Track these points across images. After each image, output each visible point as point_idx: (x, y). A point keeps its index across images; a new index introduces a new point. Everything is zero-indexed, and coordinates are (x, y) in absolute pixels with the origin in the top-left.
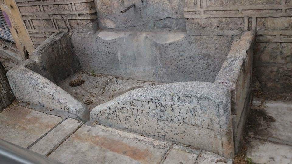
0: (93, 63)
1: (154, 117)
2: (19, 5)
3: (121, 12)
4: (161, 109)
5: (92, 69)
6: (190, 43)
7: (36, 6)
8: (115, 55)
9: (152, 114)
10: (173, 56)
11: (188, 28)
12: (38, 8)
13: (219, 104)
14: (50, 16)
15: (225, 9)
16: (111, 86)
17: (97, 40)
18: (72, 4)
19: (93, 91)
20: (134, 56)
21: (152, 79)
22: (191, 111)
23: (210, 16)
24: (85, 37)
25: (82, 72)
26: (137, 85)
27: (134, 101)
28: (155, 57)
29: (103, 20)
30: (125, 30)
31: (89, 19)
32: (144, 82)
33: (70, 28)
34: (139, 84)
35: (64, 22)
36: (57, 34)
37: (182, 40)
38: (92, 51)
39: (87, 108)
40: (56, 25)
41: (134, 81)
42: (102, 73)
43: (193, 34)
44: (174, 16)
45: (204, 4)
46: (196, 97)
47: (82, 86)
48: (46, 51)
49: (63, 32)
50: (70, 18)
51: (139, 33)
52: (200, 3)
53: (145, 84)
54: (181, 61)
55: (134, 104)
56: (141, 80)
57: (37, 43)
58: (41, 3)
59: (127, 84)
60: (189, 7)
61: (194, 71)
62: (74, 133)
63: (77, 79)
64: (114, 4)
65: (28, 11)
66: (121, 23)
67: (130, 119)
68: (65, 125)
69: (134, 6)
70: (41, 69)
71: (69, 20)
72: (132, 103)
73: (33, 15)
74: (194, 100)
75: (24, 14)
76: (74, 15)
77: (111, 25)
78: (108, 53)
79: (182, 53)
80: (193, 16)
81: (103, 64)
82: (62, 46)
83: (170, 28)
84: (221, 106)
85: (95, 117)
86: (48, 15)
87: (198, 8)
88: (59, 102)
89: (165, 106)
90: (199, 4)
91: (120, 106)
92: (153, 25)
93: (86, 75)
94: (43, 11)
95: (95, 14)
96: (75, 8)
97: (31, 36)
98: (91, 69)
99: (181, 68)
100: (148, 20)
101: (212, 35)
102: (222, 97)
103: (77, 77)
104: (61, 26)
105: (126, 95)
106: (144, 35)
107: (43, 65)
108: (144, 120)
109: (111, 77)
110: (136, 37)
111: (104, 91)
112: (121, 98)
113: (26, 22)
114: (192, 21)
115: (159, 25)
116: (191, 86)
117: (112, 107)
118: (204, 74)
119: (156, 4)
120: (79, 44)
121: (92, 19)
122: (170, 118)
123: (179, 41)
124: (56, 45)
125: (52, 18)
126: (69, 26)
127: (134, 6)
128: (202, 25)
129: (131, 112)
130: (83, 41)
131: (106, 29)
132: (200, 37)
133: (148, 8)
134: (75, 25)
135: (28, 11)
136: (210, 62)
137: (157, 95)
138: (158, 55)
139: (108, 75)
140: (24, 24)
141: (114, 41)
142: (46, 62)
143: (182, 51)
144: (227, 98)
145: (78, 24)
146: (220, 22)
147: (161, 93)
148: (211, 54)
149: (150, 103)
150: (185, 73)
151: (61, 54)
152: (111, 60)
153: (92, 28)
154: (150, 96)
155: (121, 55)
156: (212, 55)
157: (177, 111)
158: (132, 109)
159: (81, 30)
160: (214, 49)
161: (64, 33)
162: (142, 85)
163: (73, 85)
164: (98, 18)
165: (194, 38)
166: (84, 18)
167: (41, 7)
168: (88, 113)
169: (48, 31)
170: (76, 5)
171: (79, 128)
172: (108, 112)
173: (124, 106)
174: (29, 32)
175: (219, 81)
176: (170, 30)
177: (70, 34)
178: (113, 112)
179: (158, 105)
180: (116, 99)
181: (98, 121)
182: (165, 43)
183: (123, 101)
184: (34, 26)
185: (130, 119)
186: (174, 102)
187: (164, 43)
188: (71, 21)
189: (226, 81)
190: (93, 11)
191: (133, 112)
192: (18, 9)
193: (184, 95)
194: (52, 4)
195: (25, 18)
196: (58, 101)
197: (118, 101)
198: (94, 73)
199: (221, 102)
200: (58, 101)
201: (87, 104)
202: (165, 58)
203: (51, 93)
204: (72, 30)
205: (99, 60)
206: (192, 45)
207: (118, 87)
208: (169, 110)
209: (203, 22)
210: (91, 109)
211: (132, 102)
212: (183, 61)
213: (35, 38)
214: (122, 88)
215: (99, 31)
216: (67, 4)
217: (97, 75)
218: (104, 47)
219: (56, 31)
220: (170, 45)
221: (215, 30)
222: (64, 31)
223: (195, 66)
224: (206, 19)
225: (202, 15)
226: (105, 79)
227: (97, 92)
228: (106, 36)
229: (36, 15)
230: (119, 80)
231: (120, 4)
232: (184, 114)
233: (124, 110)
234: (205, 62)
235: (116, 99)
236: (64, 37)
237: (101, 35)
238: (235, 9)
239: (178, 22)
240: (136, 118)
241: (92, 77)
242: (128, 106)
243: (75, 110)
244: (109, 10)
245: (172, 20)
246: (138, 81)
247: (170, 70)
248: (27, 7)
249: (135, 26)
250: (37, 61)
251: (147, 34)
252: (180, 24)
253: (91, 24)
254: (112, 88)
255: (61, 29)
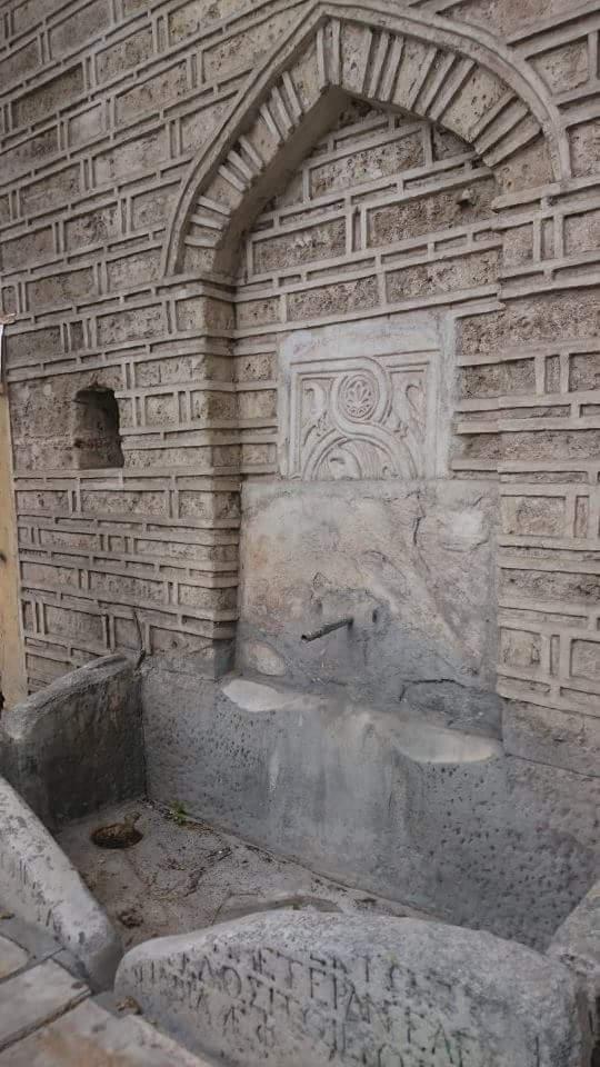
0: (188, 775)
1: (322, 1033)
2: (25, 557)
3: (304, 637)
4: (348, 1010)
5: (180, 796)
6: (512, 782)
7: (70, 569)
8: (262, 764)
9: (315, 1019)
10: (449, 814)
11: (505, 728)
12: (75, 577)
13: (540, 1039)
14: (103, 605)
16: (222, 874)
17: (216, 704)
18: (171, 584)
19: (159, 878)
20: (321, 781)
21: (368, 881)
22: (448, 1045)
24: (185, 687)
25: (146, 800)
26: (314, 891)
27: (265, 954)
28: (391, 801)
29: (251, 645)
30: (309, 687)
31: (211, 636)
32: (339, 886)
33: (148, 651)
34: (320, 888)
35: (135, 631)
36: (105, 664)
37: (487, 766)
39: (117, 938)
41: (305, 874)
42: (205, 817)
43: (521, 752)
44: (468, 680)
46: (468, 991)
47: (130, 853)
48: (56, 711)
49: (125, 659)
51: (349, 709)
53: (341, 892)
54: (475, 839)
55: (264, 966)
56: (331, 874)
57: (38, 677)
59: (278, 877)
60: (517, 666)
61: (518, 888)
62: (47, 1022)
63: (123, 822)
64: (291, 605)
65: (44, 579)
67: (242, 1019)
68: (28, 986)
70: (20, 768)
71: (152, 627)
72: (257, 958)
73: (55, 593)
74: (462, 1003)
75: (28, 584)
79: (480, 810)
80: (526, 697)
81: (216, 787)
82: (110, 702)
83: (451, 713)
84: (545, 1050)
85: (131, 978)
86: (95, 601)
87: (542, 676)
88: (39, 894)
89: (362, 1001)
90: (545, 664)
91: (218, 961)
92: (398, 693)
93: (156, 814)
95: (233, 624)
97: (29, 651)
98: (175, 796)
99: (476, 863)
102: (552, 1015)
103: (123, 814)
105: (246, 924)
106: (365, 718)
107: (30, 753)
108: (290, 1039)
109: (232, 840)
110: (340, 718)
111: (194, 886)
112: (227, 932)
113: (28, 606)
114: (522, 712)
116: (461, 946)
117: (191, 958)
118: (554, 906)
119: (413, 632)
121: (216, 637)
122: (375, 1054)
123: (473, 765)
124: (91, 697)
126: (146, 646)
127: (350, 623)
128: (554, 732)
129: (250, 995)
131: (255, 674)
132: (545, 768)
134: (166, 645)
135: (44, 579)
136: (577, 869)
137: (343, 952)
138: (401, 797)
139: (225, 831)
140: (21, 612)
141: (268, 717)
142: (43, 749)
143: (483, 803)
144: (571, 1021)
145: (175, 644)
147: (359, 945)
148: (578, 837)
149: (318, 977)
150: (485, 885)
151: (96, 729)
152: (247, 777)
153: (212, 665)
154: (321, 948)
155: (281, 769)
156: (583, 842)
157: (400, 1029)
158: (255, 984)
159: (177, 665)
161: (125, 663)
162: (332, 897)
163: (105, 841)
165: (525, 769)
167: (85, 575)
168: (114, 956)
169: (81, 646)
170: (183, 588)
171: (69, 1007)
172: (177, 974)
173: (232, 963)
174: (26, 638)
175: (561, 951)
176: (451, 722)
177: (144, 669)
178: (193, 976)
179: (341, 991)
180: (211, 932)
181: (138, 999)
182: (427, 760)
183: (231, 944)
184: (48, 623)
185: (242, 1019)
186: (396, 994)
187: (424, 759)
189: (583, 957)
190: (228, 616)
191: (254, 995)
192: (18, 567)
193: (431, 974)
195: (28, 597)
196: (37, 890)
197: (216, 941)
198: (182, 812)
199: (549, 1033)
200: (37, 890)
201: (124, 923)
203: (24, 858)
206: (516, 790)
207: (247, 885)
208: (376, 1018)
209: (558, 722)
210: (130, 943)
211: (260, 956)
212: (484, 838)
213: (40, 661)
215: (229, 676)
216: (159, 583)
217: (191, 823)
218: (232, 728)
219: (106, 651)
220: (443, 770)
222: (129, 656)
223: (522, 868)
224: (566, 716)
225: (554, 699)
226: (211, 843)
227: (172, 884)
228: (248, 697)
230: (254, 858)
231: (308, 611)
232: (424, 1049)
233: (227, 978)
234: (560, 860)
235: (212, 931)
236: (123, 676)
237: (234, 690)
239: (481, 703)
240: (261, 1022)
241: (172, 826)
242: (243, 967)
243: (78, 938)
244: (274, 622)
246: (318, 878)
247: (435, 861)
248: (43, 567)
249: (344, 684)
250: (17, 736)
252: (486, 710)
253: (211, 653)
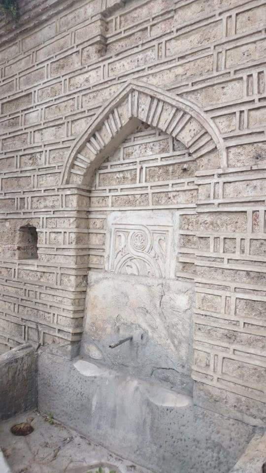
3: (110, 346)
5: (51, 410)
6: (196, 417)
7: (10, 303)
8: (89, 400)
11: (195, 393)
12: (12, 307)
15: (246, 384)
17: (70, 371)
18: (54, 314)
21: (133, 457)
23: (226, 387)
24: (57, 361)
28: (145, 422)
30: (111, 367)
31: (70, 340)
33: (42, 344)
35: (37, 333)
38: (60, 384)
40: (26, 334)
41: (105, 451)
42: (63, 421)
44: (180, 369)
45: (219, 368)
47: (27, 438)
50: (46, 331)
51: (129, 378)
52: (214, 366)
53: (121, 462)
56: (117, 453)
58: (18, 302)
61: (197, 466)
63: (26, 422)
66: (109, 356)
69: (131, 339)
76: (53, 329)
77: (95, 354)
78: (79, 394)
80: (204, 381)
81: (68, 408)
82: (23, 366)
83: (172, 383)
86: (20, 319)
92: (150, 372)
94: (17, 312)
95: (80, 334)
96: (57, 321)
100: (146, 363)
101: (227, 415)
104: (32, 338)
109: (74, 433)
114: (202, 387)
115: (159, 374)
120: (46, 369)
121: (74, 340)
123: (180, 408)
124: (15, 364)
125: (24, 324)
128: (214, 397)
130: (53, 366)
131: (87, 358)
132: (210, 412)
133: (147, 348)
134: (50, 342)
136: (222, 459)
138: (149, 421)
139: (71, 428)
141: (93, 379)
145: (54, 342)
146: (239, 400)
148: (223, 444)
152: (82, 405)
159: (54, 351)
160: (228, 438)
161: (32, 348)
164: (82, 341)
166: (64, 337)
169: (13, 338)
176: (172, 387)
177: (39, 351)
182: (161, 405)
187: (159, 404)
188: (47, 335)
190: (78, 331)
194: (30, 307)
198: (52, 418)
202: (157, 428)
204: (43, 348)
205: (65, 400)
209: (216, 393)
214: (84, 459)
215: (78, 358)
217: (56, 423)
220: (167, 410)
221: (231, 409)
222: (33, 345)
223: (199, 456)
224: (220, 391)
225: (215, 383)
226: (65, 434)
228: (85, 369)
229: (6, 314)
234: (215, 455)
236: (29, 355)
237: (79, 365)
238: (259, 389)
241: (47, 424)
245: (177, 374)
247: (162, 450)
249: (127, 366)
251: (140, 384)
253: (70, 347)
254: (68, 455)
255: (30, 342)
